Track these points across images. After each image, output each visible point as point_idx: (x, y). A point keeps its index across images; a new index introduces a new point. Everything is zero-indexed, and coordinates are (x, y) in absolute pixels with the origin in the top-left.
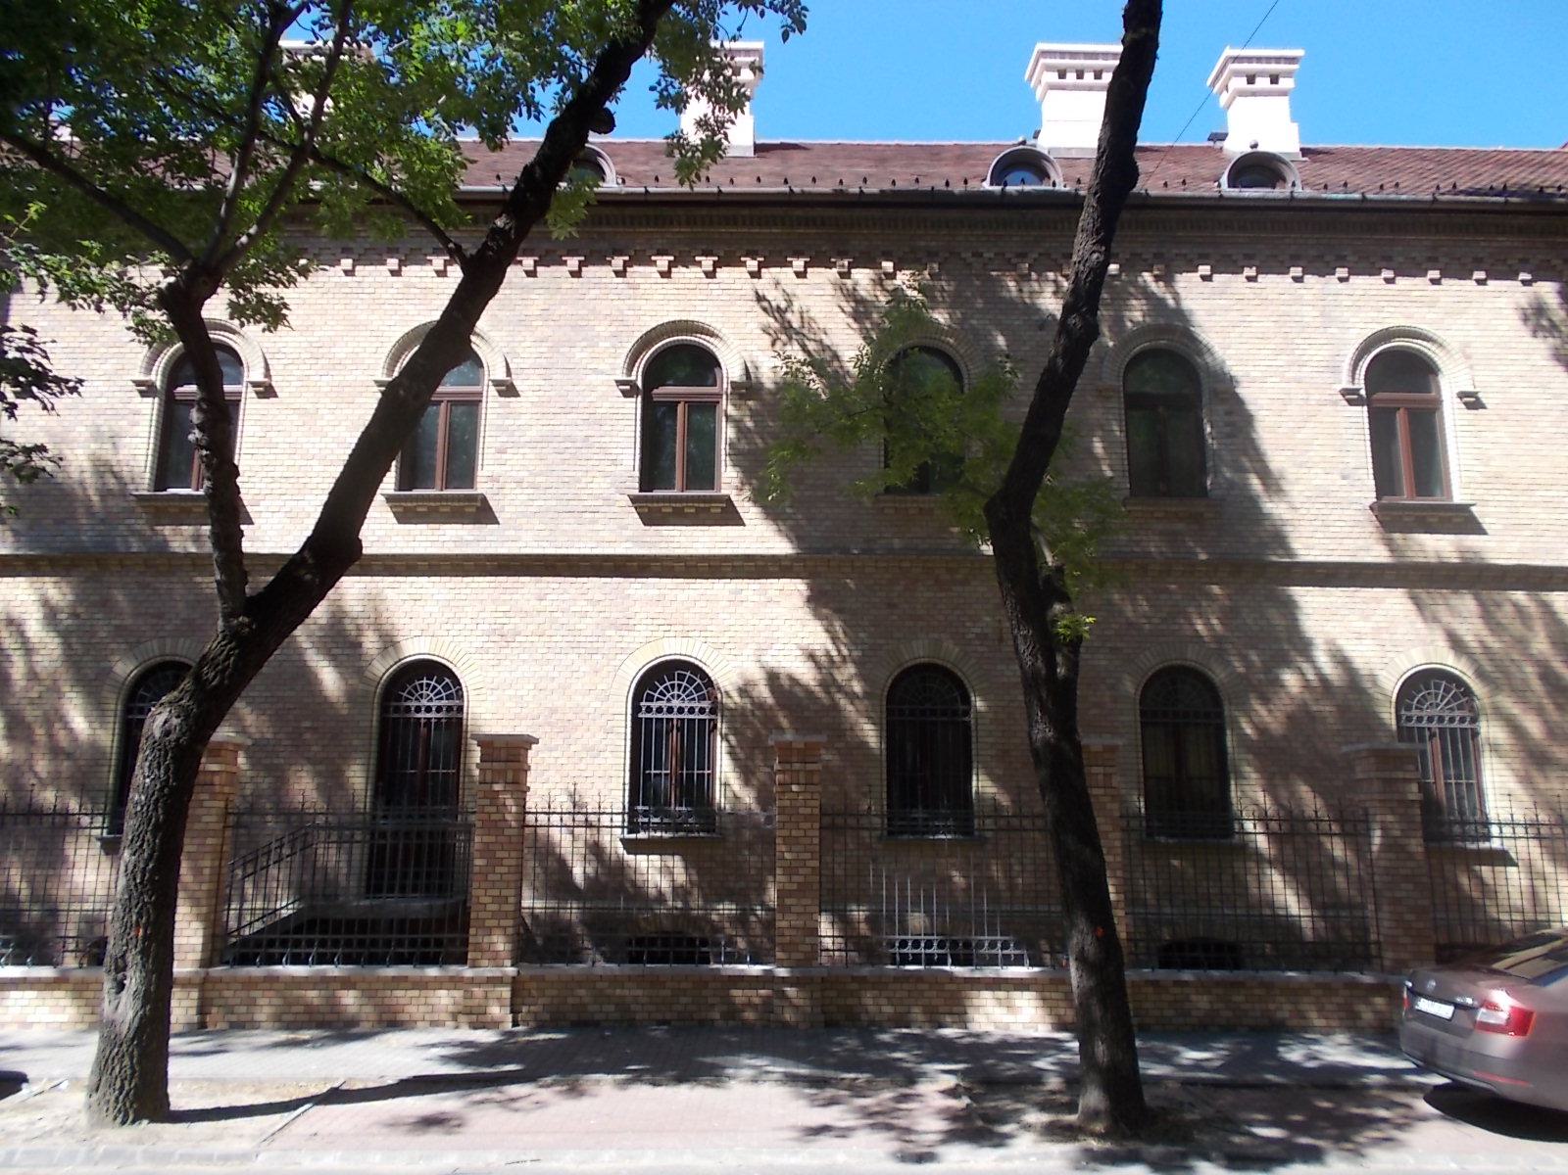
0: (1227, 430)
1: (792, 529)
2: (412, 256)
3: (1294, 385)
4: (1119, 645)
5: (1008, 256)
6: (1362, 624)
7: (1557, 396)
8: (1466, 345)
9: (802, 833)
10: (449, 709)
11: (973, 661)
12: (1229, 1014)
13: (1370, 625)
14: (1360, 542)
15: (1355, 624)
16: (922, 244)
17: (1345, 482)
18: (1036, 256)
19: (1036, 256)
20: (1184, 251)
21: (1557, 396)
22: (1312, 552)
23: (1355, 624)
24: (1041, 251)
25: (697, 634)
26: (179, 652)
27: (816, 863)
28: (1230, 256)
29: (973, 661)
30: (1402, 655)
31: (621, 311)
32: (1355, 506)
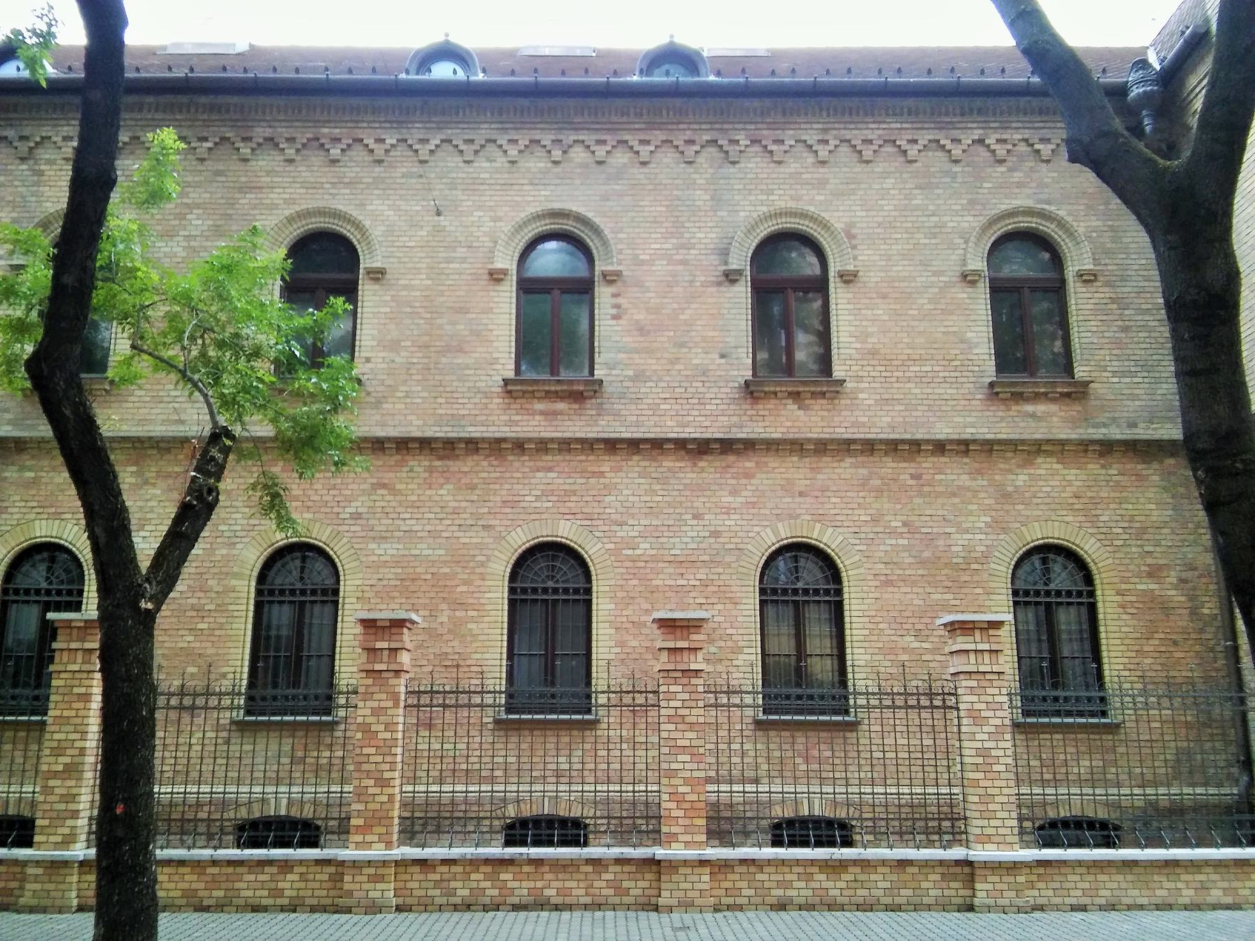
0: (614, 311)
1: (1234, 373)
2: (1014, 37)
3: (680, 268)
4: (491, 523)
5: (410, 142)
6: (731, 499)
7: (935, 274)
8: (851, 225)
9: (73, 713)
10: (70, 593)
11: (345, 540)
12: (503, 876)
13: (739, 499)
14: (735, 419)
15: (724, 499)
16: (326, 130)
17: (723, 361)
18: (438, 142)
19: (438, 142)
20: (581, 138)
21: (935, 274)
22: (687, 430)
23: (724, 499)
24: (443, 137)
25: (69, 516)
26: (65, 537)
27: (1010, 760)
28: (626, 142)
29: (345, 540)
30: (768, 530)
31: (23, 197)
32: (731, 384)
